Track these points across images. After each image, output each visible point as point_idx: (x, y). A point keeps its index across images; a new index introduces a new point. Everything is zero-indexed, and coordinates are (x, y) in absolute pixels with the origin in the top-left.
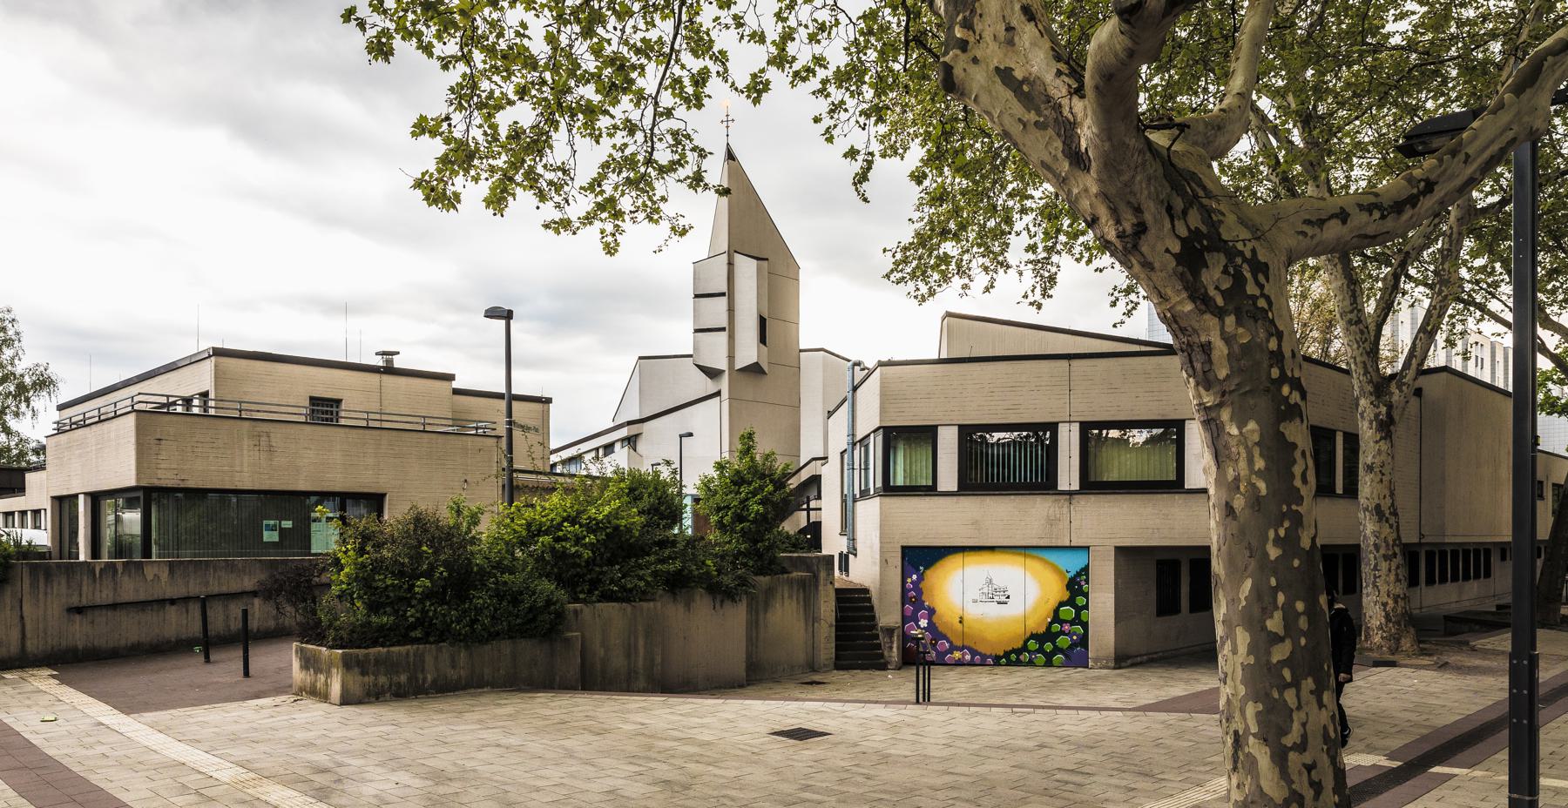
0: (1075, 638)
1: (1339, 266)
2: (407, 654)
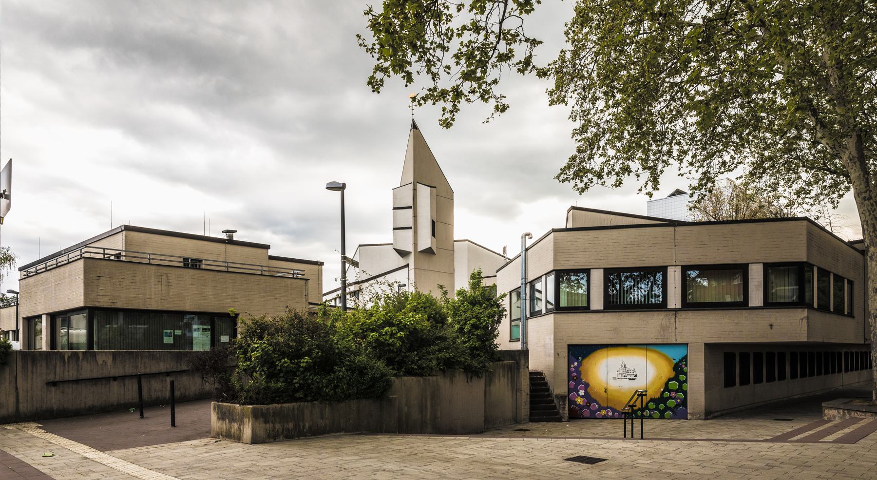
0: (679, 401)
1: (858, 163)
2: (293, 408)
